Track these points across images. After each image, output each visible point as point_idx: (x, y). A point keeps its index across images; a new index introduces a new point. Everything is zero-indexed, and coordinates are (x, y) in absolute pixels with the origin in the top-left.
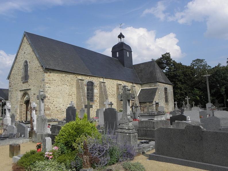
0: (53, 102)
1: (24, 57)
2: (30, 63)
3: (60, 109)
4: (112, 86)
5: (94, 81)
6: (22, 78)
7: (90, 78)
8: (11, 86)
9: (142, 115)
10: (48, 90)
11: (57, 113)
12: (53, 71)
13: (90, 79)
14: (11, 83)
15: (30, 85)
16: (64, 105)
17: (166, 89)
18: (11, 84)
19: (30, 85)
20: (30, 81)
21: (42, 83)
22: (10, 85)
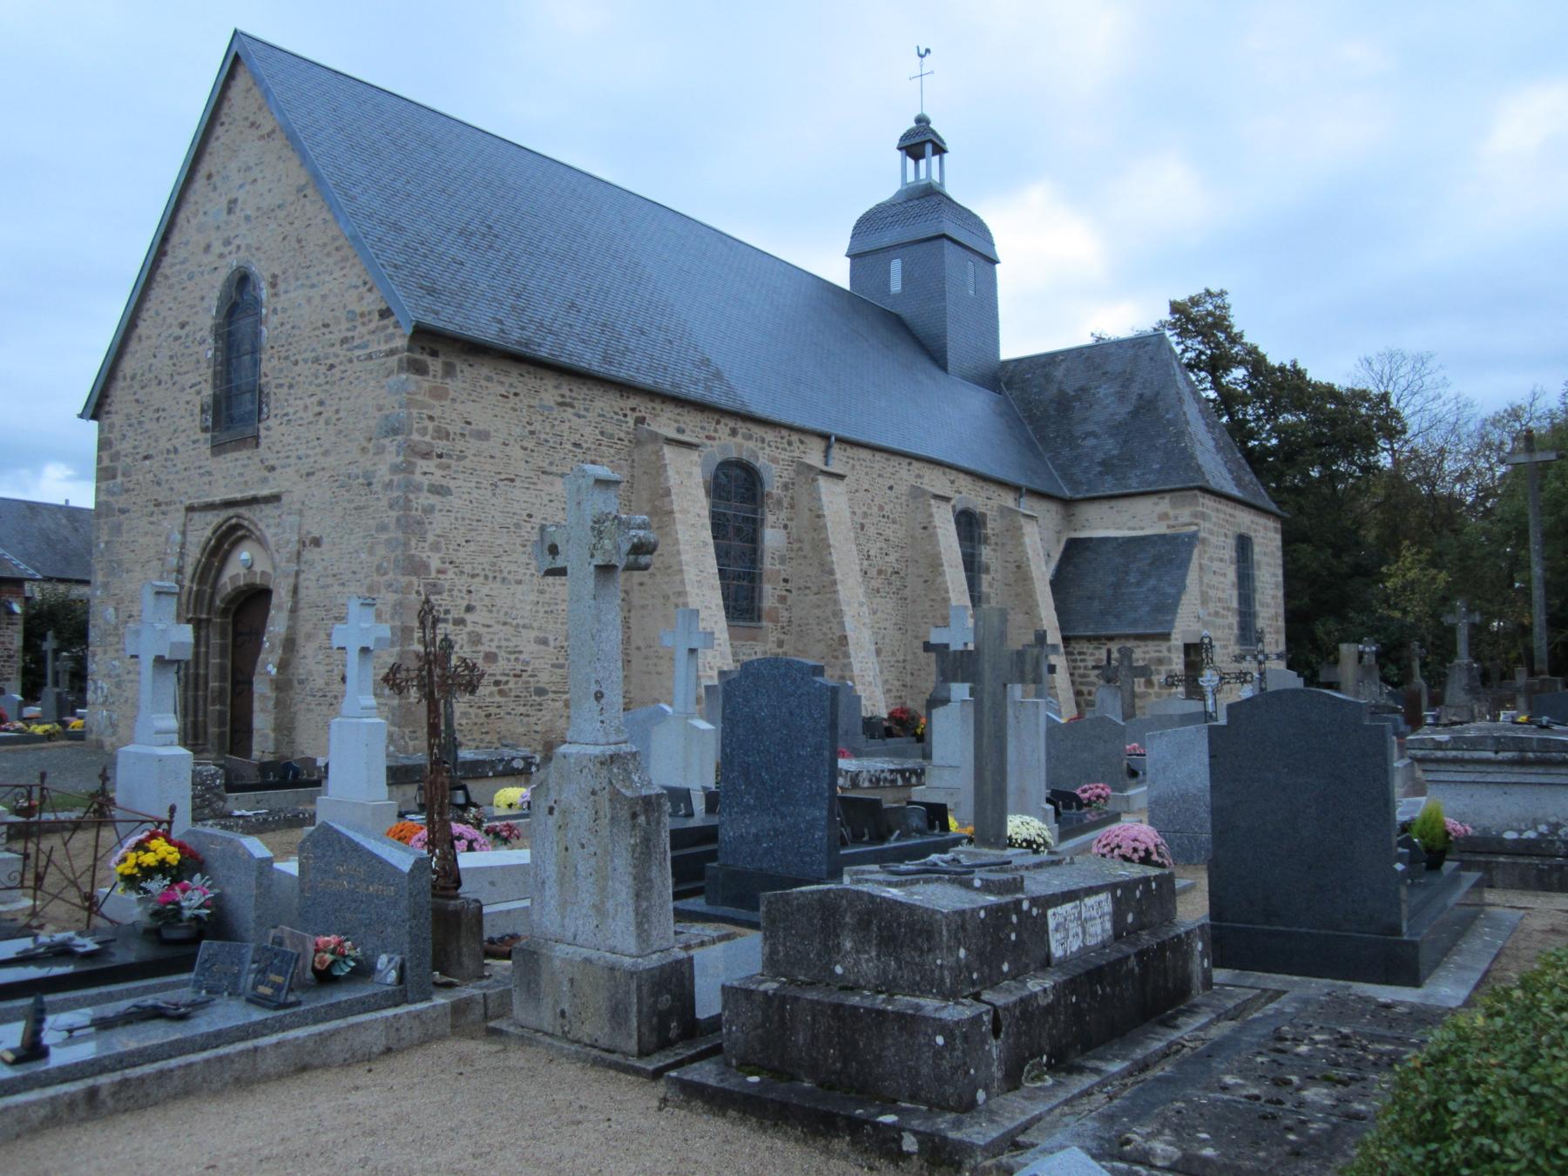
0: (469, 609)
1: (227, 243)
2: (274, 285)
3: (519, 667)
4: (881, 508)
5: (762, 462)
6: (203, 411)
7: (734, 432)
8: (114, 469)
9: (1438, 761)
10: (429, 510)
11: (498, 699)
12: (471, 360)
13: (739, 439)
14: (117, 447)
15: (272, 469)
16: (544, 642)
17: (1244, 545)
18: (115, 457)
19: (272, 469)
20: (273, 430)
21: (381, 450)
22: (106, 463)
